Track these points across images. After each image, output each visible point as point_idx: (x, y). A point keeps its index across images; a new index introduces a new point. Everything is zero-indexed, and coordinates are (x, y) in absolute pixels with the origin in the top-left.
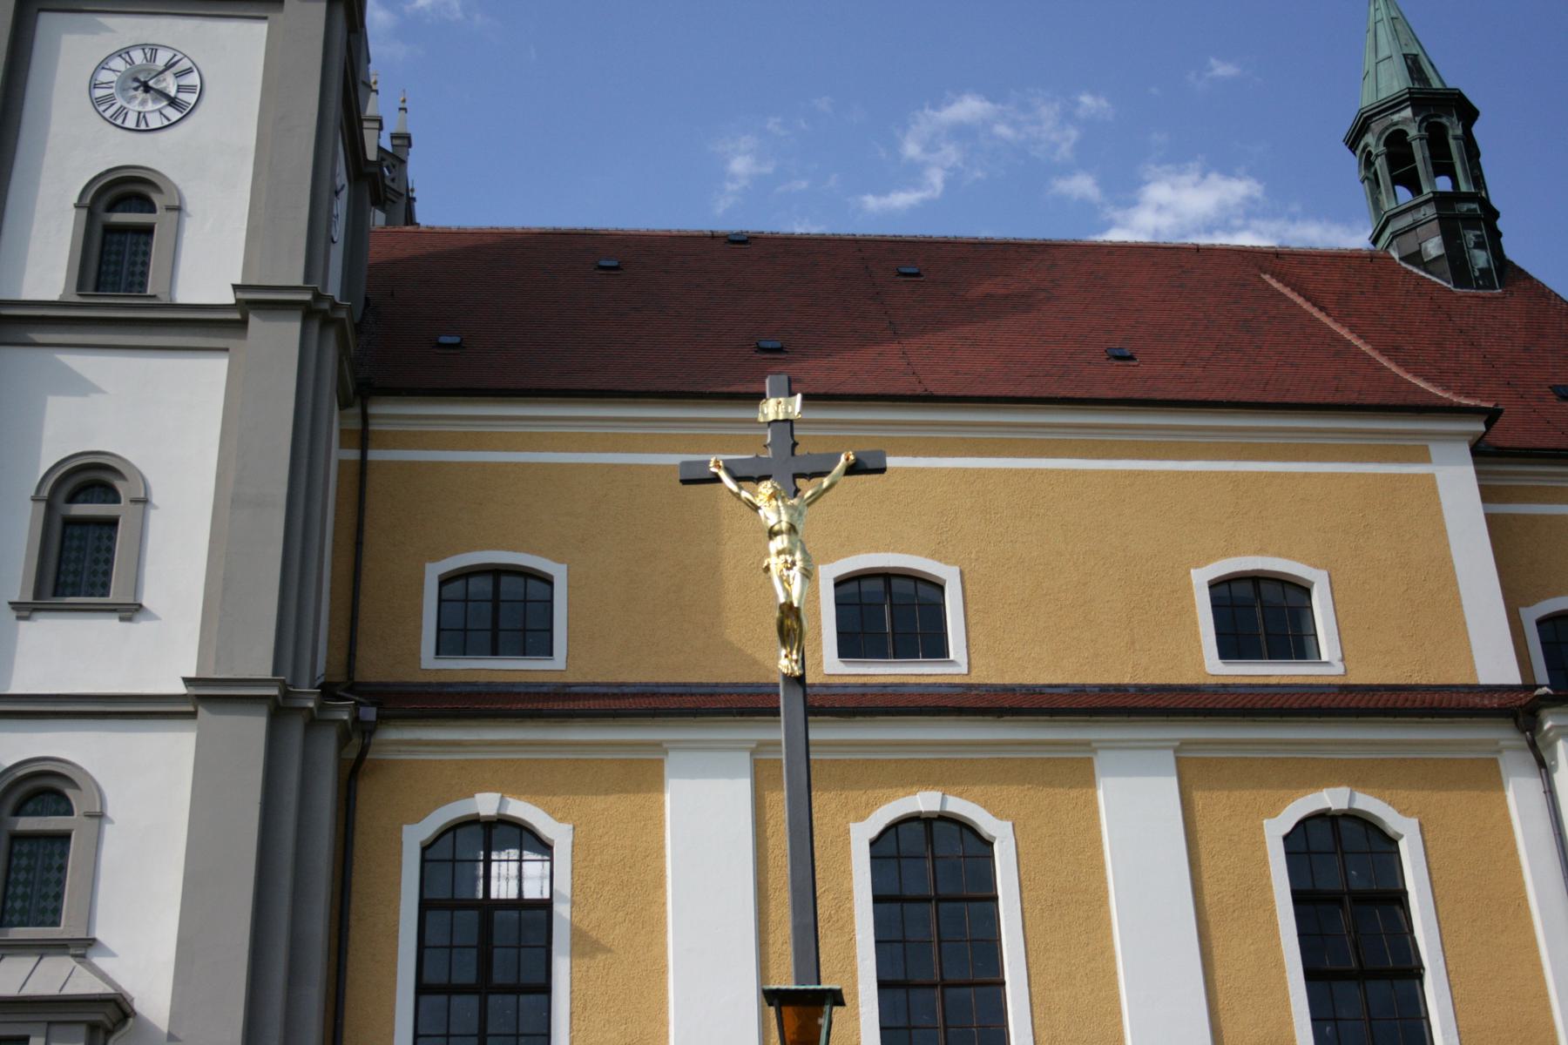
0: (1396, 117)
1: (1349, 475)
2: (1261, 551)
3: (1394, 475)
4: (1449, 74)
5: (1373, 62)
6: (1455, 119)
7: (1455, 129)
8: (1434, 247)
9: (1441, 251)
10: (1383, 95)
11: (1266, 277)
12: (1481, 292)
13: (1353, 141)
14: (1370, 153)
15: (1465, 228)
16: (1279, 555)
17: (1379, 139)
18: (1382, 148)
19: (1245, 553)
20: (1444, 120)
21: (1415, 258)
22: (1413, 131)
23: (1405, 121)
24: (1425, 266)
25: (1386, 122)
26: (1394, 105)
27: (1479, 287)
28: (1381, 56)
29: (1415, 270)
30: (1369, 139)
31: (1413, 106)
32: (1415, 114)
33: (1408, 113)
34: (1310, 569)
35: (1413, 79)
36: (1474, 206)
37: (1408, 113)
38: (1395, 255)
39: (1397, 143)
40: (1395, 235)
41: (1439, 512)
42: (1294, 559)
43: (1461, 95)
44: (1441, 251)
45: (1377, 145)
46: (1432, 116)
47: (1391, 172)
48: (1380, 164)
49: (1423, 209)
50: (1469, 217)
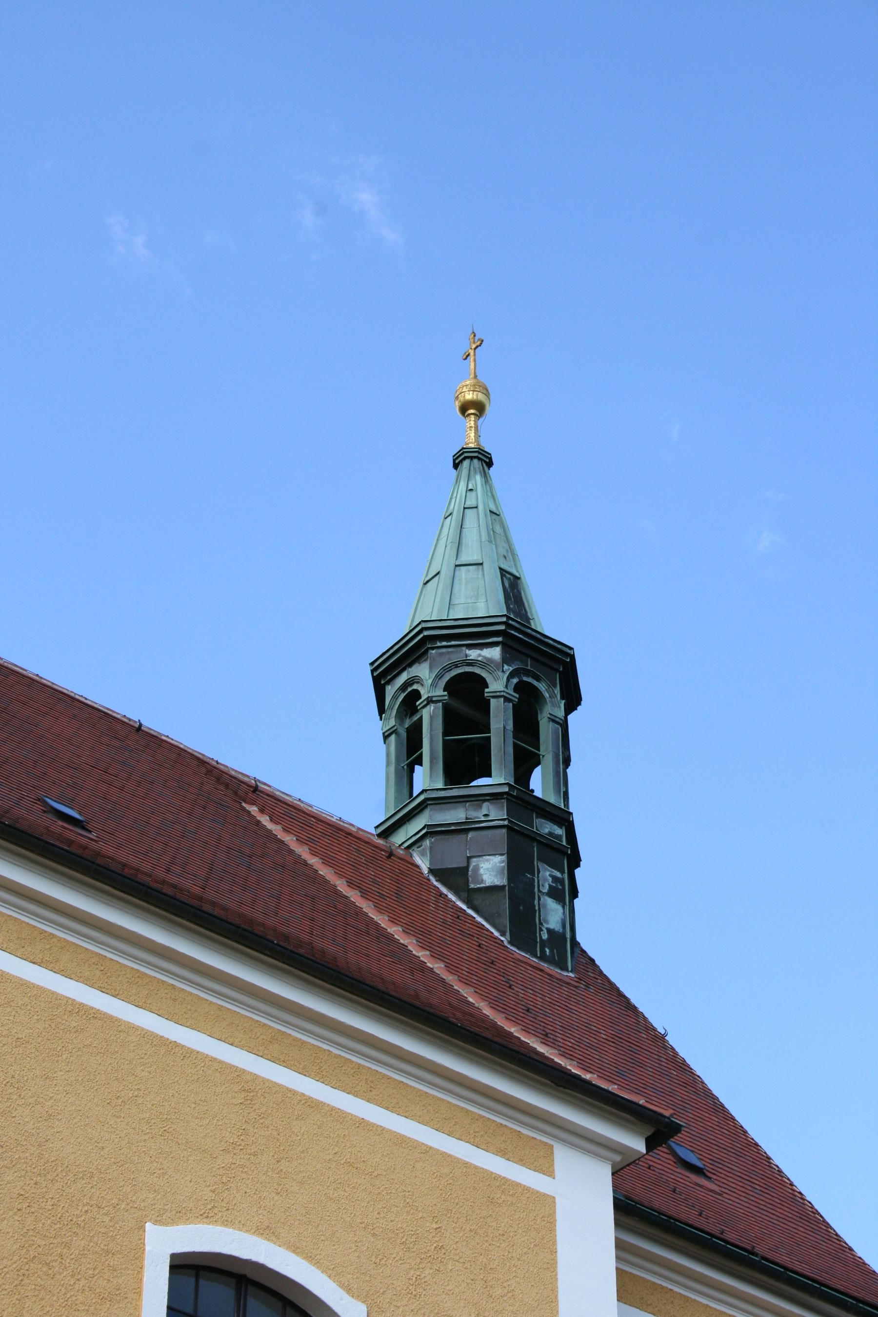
0: (473, 654)
1: (428, 1150)
2: (266, 1231)
3: (496, 1177)
4: (550, 620)
5: (453, 562)
6: (557, 691)
7: (554, 707)
8: (490, 870)
9: (499, 880)
10: (459, 613)
11: (253, 809)
12: (544, 965)
13: (383, 673)
14: (416, 695)
15: (541, 859)
16: (295, 1249)
17: (439, 677)
18: (440, 692)
19: (242, 1226)
20: (542, 686)
21: (456, 877)
22: (497, 684)
23: (486, 664)
24: (471, 896)
25: (457, 656)
26: (474, 633)
27: (543, 958)
28: (464, 559)
29: (451, 897)
30: (423, 671)
31: (505, 646)
32: (505, 660)
33: (495, 653)
34: (342, 1293)
35: (508, 609)
36: (560, 831)
37: (495, 653)
38: (423, 864)
39: (466, 690)
40: (431, 831)
41: (552, 1266)
42: (317, 1264)
43: (573, 657)
44: (499, 880)
45: (434, 685)
46: (528, 673)
47: (445, 734)
48: (430, 718)
49: (486, 808)
50: (545, 843)
